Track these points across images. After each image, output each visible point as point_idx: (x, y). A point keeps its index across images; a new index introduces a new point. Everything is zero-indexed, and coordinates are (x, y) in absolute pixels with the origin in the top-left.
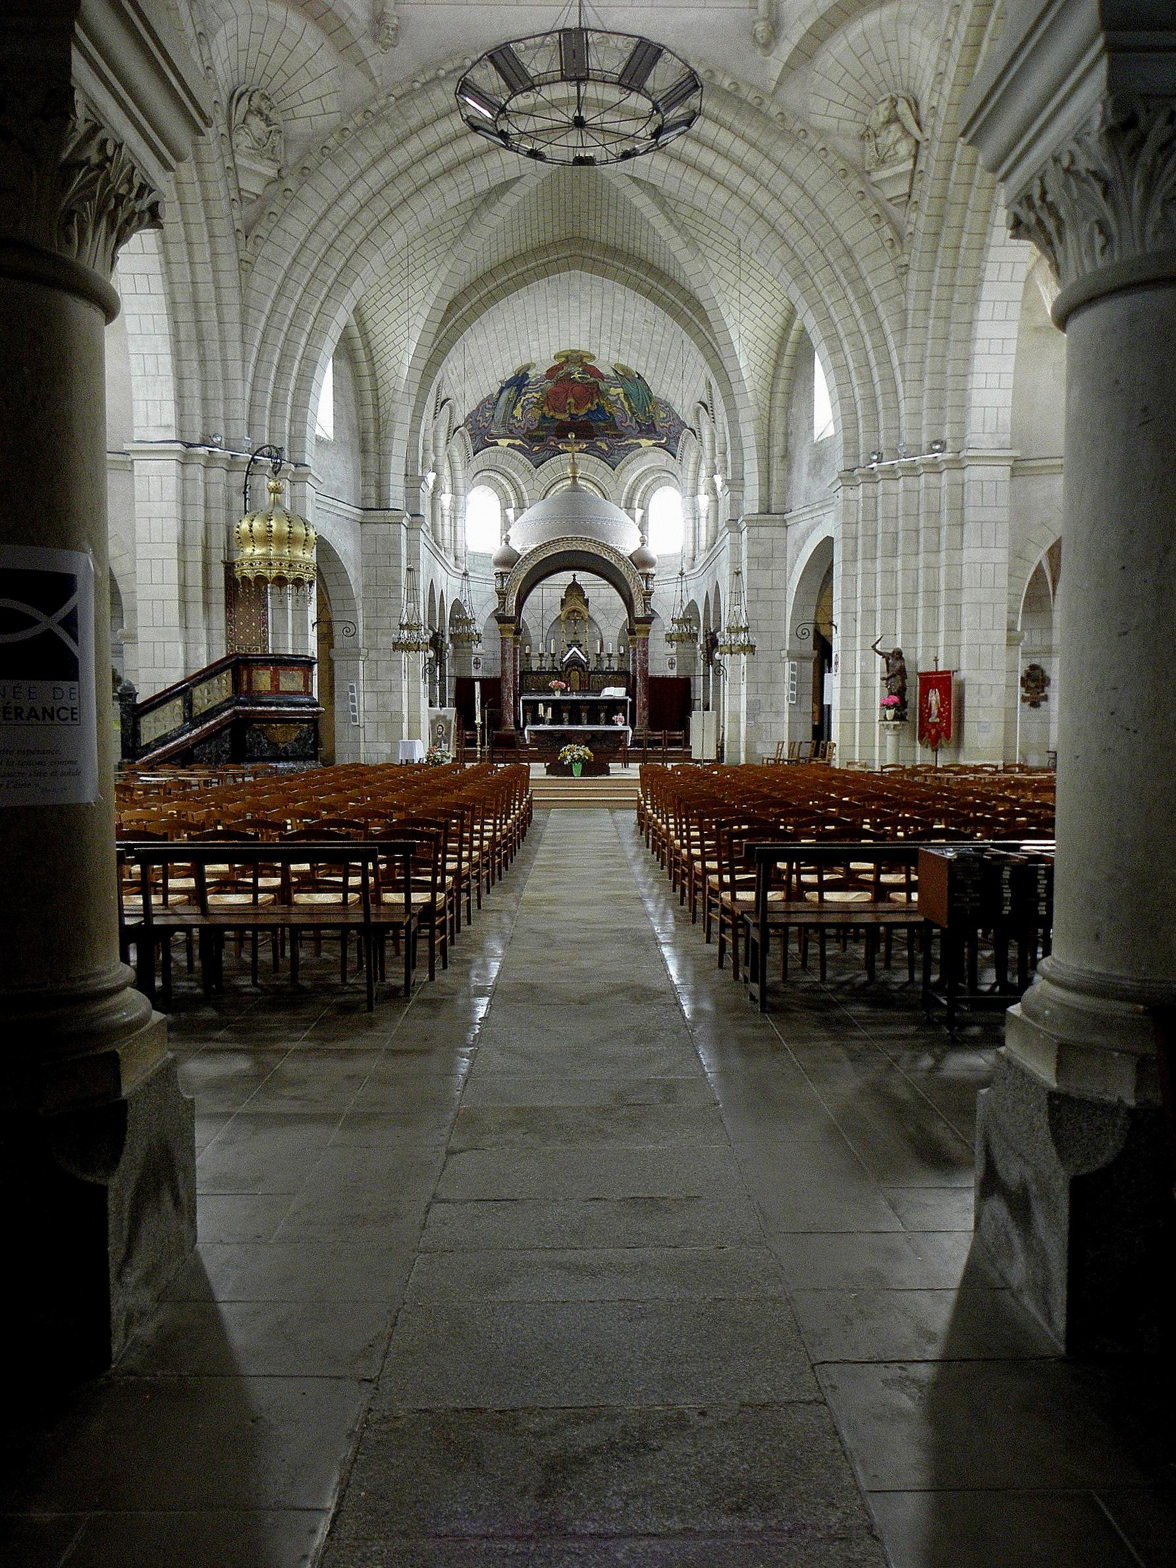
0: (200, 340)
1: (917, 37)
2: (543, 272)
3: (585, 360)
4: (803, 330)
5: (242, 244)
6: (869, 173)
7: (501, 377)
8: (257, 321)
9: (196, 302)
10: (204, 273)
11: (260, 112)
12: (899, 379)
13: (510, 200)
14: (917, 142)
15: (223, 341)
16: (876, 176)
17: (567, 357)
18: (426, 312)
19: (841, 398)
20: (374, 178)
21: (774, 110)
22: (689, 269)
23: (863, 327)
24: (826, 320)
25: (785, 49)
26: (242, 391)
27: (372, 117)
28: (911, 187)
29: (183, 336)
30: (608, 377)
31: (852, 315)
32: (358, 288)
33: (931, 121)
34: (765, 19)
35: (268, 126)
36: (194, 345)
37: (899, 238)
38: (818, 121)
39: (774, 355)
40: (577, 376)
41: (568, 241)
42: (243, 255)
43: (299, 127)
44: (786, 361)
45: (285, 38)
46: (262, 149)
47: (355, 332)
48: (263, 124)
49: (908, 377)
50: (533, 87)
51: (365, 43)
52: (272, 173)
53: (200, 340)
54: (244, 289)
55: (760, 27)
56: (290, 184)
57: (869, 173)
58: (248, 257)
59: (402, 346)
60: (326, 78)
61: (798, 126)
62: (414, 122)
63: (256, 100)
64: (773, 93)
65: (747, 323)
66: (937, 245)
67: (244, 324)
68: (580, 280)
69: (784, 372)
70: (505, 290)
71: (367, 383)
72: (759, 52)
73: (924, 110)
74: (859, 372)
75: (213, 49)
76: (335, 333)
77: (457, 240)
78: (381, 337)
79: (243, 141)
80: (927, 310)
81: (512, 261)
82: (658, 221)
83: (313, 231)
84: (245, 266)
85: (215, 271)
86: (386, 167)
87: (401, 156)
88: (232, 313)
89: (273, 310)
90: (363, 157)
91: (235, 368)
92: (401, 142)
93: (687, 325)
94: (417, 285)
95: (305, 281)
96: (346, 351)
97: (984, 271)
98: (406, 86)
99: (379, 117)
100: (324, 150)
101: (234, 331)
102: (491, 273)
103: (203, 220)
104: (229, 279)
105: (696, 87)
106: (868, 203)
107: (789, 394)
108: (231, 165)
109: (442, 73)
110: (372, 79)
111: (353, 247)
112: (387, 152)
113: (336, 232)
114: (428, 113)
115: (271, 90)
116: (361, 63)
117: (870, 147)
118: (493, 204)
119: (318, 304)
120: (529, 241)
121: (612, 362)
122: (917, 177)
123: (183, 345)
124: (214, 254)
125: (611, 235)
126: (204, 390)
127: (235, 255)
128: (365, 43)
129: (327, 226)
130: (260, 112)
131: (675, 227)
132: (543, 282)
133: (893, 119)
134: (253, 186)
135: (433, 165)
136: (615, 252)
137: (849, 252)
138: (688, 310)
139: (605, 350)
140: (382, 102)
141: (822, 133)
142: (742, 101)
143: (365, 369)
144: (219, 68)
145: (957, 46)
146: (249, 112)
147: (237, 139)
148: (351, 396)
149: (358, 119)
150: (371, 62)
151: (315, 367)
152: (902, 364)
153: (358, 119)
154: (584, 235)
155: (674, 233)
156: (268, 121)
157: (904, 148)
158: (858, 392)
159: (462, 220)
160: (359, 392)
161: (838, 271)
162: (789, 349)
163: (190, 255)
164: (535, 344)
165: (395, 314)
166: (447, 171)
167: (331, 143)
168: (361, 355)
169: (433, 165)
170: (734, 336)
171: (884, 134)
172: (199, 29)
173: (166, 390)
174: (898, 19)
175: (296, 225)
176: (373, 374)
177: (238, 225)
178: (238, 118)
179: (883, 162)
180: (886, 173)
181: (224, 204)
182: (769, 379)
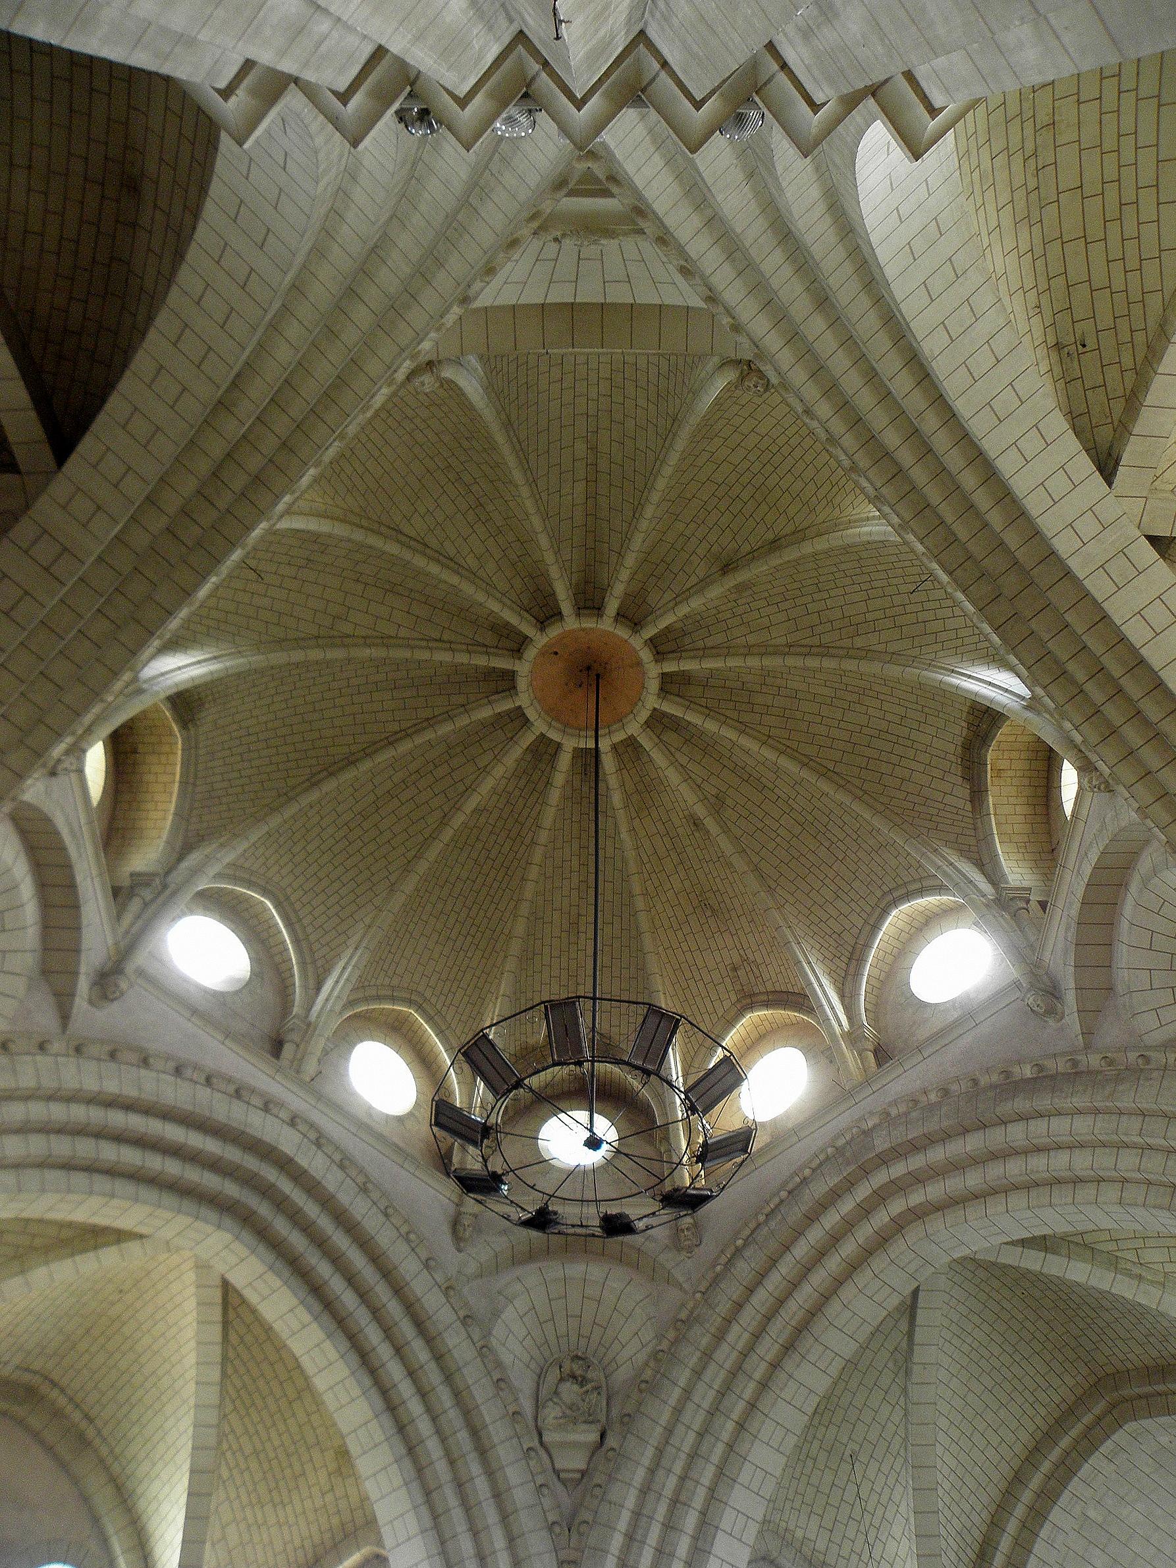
11: (573, 1377)
21: (1094, 1061)
27: (682, 1325)
34: (1029, 990)
35: (582, 1386)
42: (563, 1555)
45: (589, 1292)
46: (574, 1415)
48: (576, 1387)
51: (668, 1259)
58: (573, 1555)
60: (638, 1310)
61: (1132, 1056)
63: (567, 1366)
64: (1088, 1046)
79: (551, 1413)
90: (683, 1377)
92: (720, 1337)
98: (710, 1275)
100: (647, 1385)
109: (740, 1242)
116: (669, 1280)
120: (1043, 1412)
125: (1139, 1350)
128: (668, 1259)
130: (573, 1377)
135: (768, 1348)
140: (690, 1305)
142: (1052, 1077)
146: (562, 1380)
149: (671, 1335)
156: (582, 1381)
166: (789, 1348)
172: (462, 1313)
178: (544, 1392)
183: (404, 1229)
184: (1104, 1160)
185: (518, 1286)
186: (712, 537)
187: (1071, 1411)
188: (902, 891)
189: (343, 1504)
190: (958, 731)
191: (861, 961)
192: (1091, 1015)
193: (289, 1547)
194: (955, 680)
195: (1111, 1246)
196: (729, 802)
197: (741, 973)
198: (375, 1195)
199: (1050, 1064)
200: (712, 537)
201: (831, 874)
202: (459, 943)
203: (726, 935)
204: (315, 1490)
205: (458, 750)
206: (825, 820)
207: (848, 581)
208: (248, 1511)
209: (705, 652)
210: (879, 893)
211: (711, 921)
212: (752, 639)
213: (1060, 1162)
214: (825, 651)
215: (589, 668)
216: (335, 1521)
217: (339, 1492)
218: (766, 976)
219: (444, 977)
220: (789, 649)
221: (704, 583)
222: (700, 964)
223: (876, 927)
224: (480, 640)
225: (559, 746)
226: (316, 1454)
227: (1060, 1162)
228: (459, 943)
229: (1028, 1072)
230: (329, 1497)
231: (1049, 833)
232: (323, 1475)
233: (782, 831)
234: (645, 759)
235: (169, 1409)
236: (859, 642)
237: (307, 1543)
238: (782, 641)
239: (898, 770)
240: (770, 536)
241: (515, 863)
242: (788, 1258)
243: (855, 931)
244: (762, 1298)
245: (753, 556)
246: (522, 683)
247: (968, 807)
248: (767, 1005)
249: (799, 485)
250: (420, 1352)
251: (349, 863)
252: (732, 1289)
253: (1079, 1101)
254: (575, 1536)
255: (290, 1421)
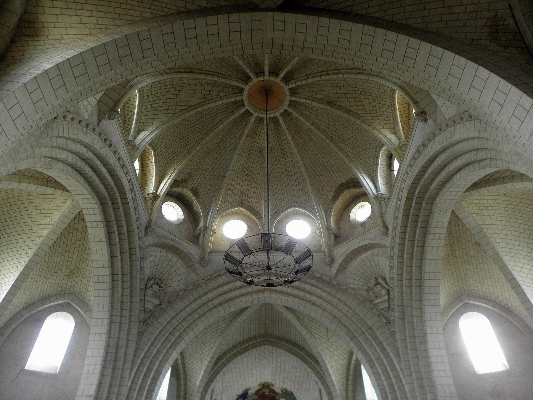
0: (115, 360)
1: (380, 259)
2: (255, 346)
3: (270, 386)
4: (357, 360)
5: (141, 326)
6: (372, 301)
7: (237, 393)
8: (140, 354)
9: (117, 346)
10: (124, 335)
11: (158, 284)
12: (402, 376)
13: (244, 317)
14: (388, 290)
15: (124, 362)
16: (375, 302)
17: (263, 385)
18: (209, 359)
19: (379, 386)
20: (194, 306)
21: (335, 283)
22: (309, 342)
23: (382, 356)
24: (366, 355)
25: (337, 265)
26: (128, 383)
27: (196, 286)
28: (389, 304)
29: (108, 358)
30: (279, 394)
31: (376, 351)
32: (182, 345)
33: (392, 281)
36: (112, 362)
37: (389, 322)
38: (351, 286)
39: (345, 376)
40: (267, 393)
41: (264, 335)
42: (140, 330)
43: (170, 289)
44: (351, 377)
46: (155, 295)
47: (180, 362)
48: (158, 287)
49: (405, 374)
50: (251, 253)
51: (197, 266)
52: (158, 303)
53: (115, 360)
54: (138, 342)
55: (327, 259)
56: (163, 306)
57: (372, 301)
59: (198, 372)
61: (345, 287)
62: (210, 287)
63: (157, 280)
64: (334, 278)
65: (333, 362)
66: (405, 323)
67: (135, 355)
68: (267, 349)
69: (350, 382)
70: (240, 353)
71: (182, 388)
72: (328, 266)
73: (388, 280)
74: (384, 374)
75: (145, 264)
76: (171, 361)
77: (222, 332)
78: (191, 369)
79: (149, 292)
80: (406, 347)
81: (243, 342)
82: (297, 324)
83: (169, 323)
84: (140, 334)
85: (128, 334)
86: (199, 302)
87: (205, 298)
88: (131, 351)
89: (147, 351)
90: (191, 298)
91: (127, 373)
92: (205, 294)
93: (310, 365)
94: (207, 349)
95: (162, 340)
96: (175, 375)
97: (426, 330)
98: (209, 277)
99: (198, 286)
100: (179, 296)
101: (130, 358)
102: (235, 347)
103: (128, 315)
104: (133, 337)
105: (310, 255)
106: (374, 310)
107: (354, 391)
108: (143, 299)
109: (222, 273)
110: (198, 275)
111: (183, 329)
112: (200, 297)
113: (177, 323)
114: (216, 285)
115: (163, 278)
116: (195, 271)
117: (371, 293)
118: (237, 319)
119: (166, 349)
121: (281, 387)
122: (391, 300)
123: (107, 362)
124: (129, 328)
126: (111, 381)
127: (137, 329)
128: (197, 266)
129: (175, 321)
130: (158, 284)
131: (303, 326)
132: (254, 350)
133: (377, 284)
134: (149, 306)
135: (216, 302)
136: (281, 339)
137: (370, 328)
138: (311, 360)
139: (278, 382)
140: (201, 281)
141: (353, 289)
143: (182, 382)
144: (146, 269)
145: (396, 257)
146: (154, 283)
147: (147, 291)
148: (175, 393)
149: (191, 287)
150: (198, 270)
151: (160, 375)
152: (401, 369)
153: (191, 287)
154: (270, 333)
155: (303, 328)
156: (160, 287)
157: (383, 292)
158: (385, 383)
159: (226, 325)
160: (178, 391)
161: (368, 335)
162: (351, 372)
163: (120, 328)
164: (251, 379)
165: (197, 360)
166: (221, 304)
167: (181, 294)
168: (182, 376)
169: (216, 302)
170: (329, 367)
171: (375, 288)
172: (141, 256)
173: (95, 380)
174: (373, 255)
175: (163, 321)
176: (185, 391)
177: (141, 319)
178: (149, 285)
179: (377, 297)
180: (378, 301)
181: (137, 311)
182: (345, 385)
183: (139, 226)
184: (324, 304)
185: (154, 253)
186: (331, 92)
187: (255, 337)
188: (295, 204)
189: (64, 285)
190: (343, 180)
191: (279, 215)
192: (339, 271)
193: (42, 291)
194: (361, 177)
195: (299, 314)
196: (273, 152)
197: (244, 195)
198: (137, 212)
199: (324, 277)
200: (331, 92)
201: (285, 188)
202: (176, 139)
203: (246, 184)
204: (58, 278)
205: (217, 85)
206: (293, 174)
207: (351, 129)
208: (36, 276)
209: (301, 114)
210: (293, 201)
211: (245, 177)
212: (315, 120)
213: (313, 298)
214: (332, 140)
215: (267, 90)
216: (59, 289)
217: (65, 281)
218: (250, 201)
219: (166, 146)
220: (323, 131)
221: (320, 101)
222: (235, 186)
223: (287, 209)
224: (251, 63)
225: (257, 77)
226: (64, 269)
227: (313, 298)
228: (176, 139)
229: (318, 275)
230: (61, 282)
231: (341, 216)
232: (63, 275)
233: (280, 168)
234: (261, 125)
235: (24, 236)
236: (341, 145)
237: (48, 292)
238: (323, 128)
239: (321, 177)
240: (348, 107)
241: (207, 127)
242: (233, 284)
243: (281, 206)
244: (221, 290)
245: (340, 108)
246: (251, 84)
247: (331, 198)
248: (246, 209)
249: (367, 104)
250: (127, 263)
251: (165, 97)
252: (214, 284)
253: (328, 290)
254: (144, 326)
255: (63, 257)
